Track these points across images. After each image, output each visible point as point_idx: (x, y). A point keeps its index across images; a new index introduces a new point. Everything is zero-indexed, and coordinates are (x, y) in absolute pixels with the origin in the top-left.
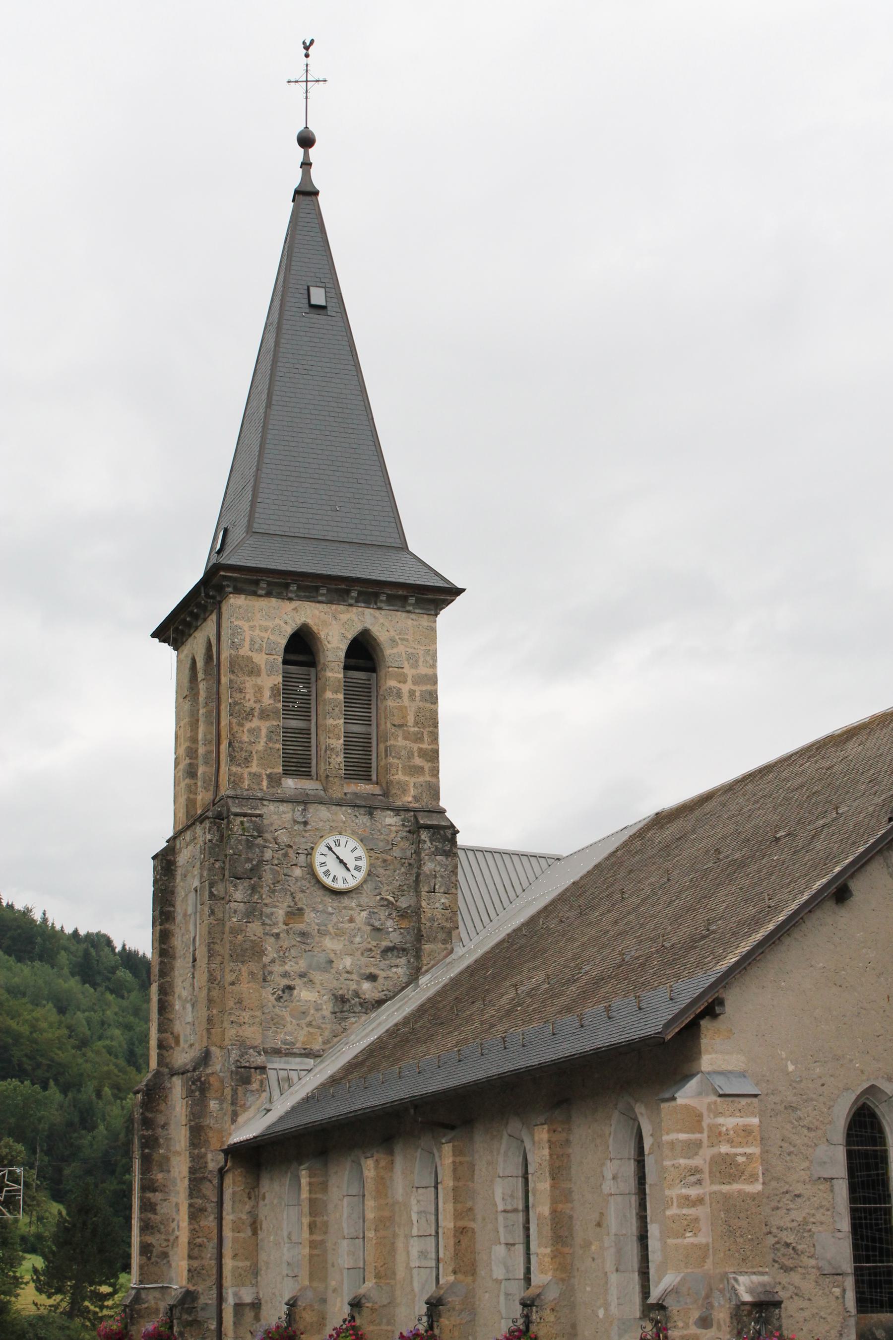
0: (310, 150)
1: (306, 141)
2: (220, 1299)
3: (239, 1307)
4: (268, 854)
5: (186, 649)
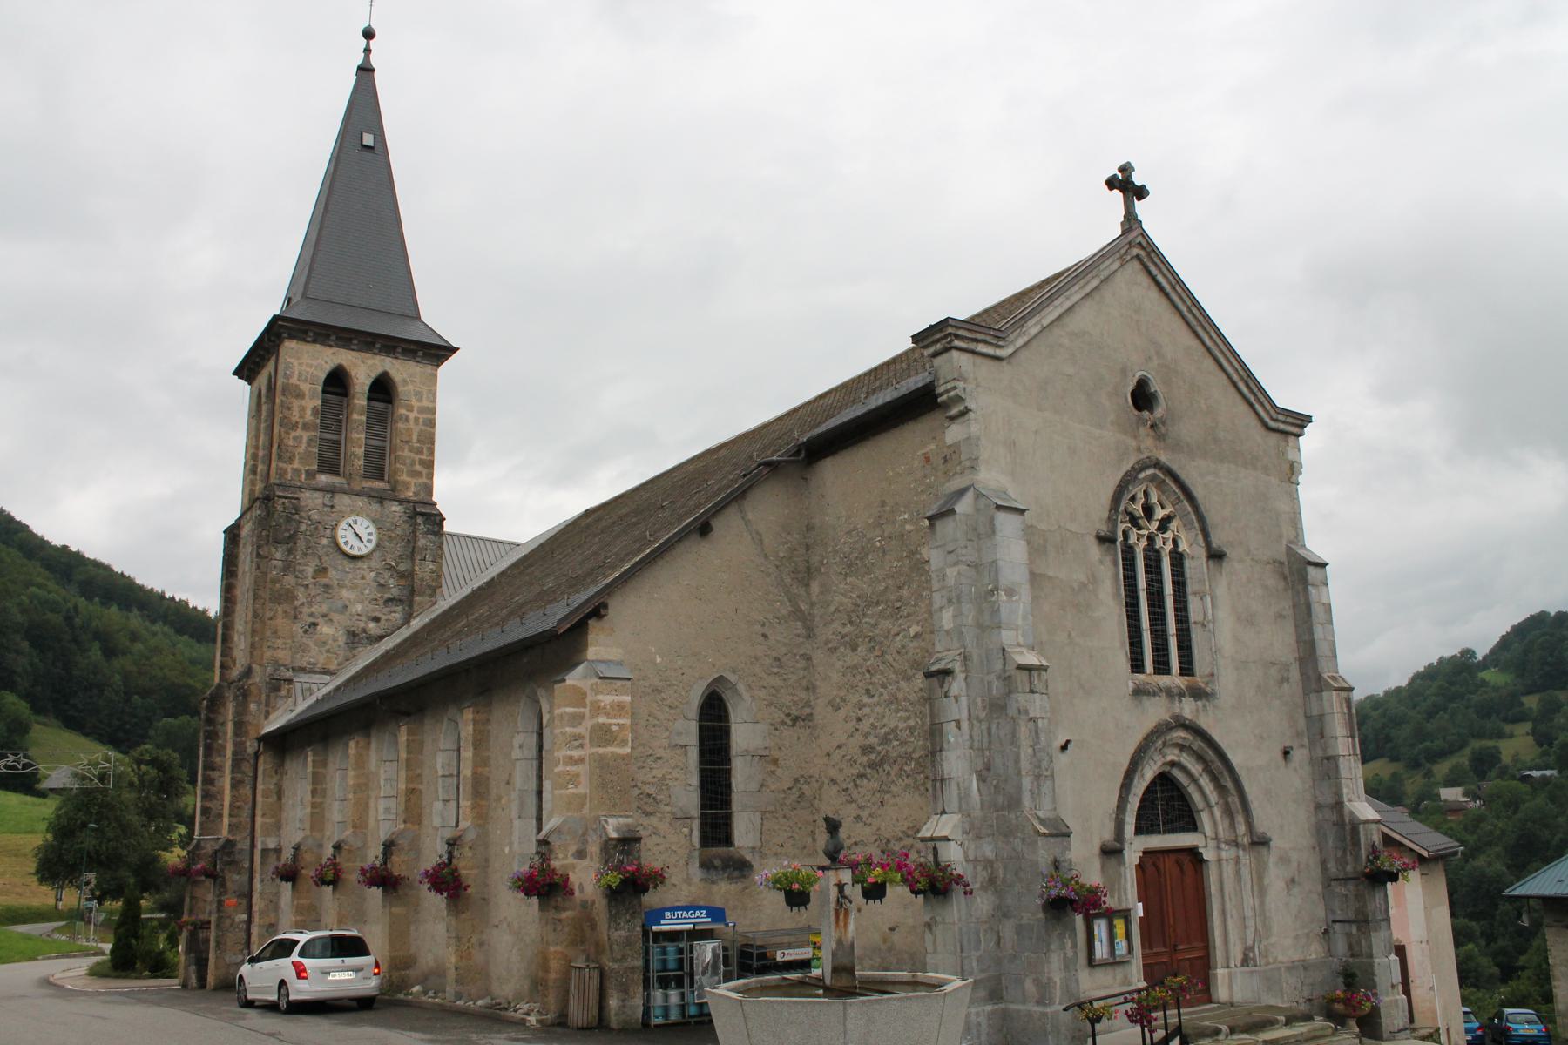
1: (369, 34)
2: (253, 845)
3: (265, 851)
4: (303, 527)
5: (256, 384)
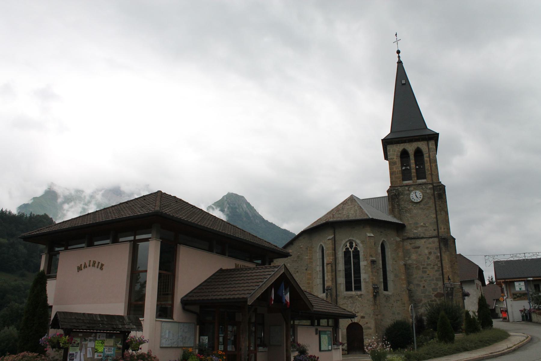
1: (398, 52)
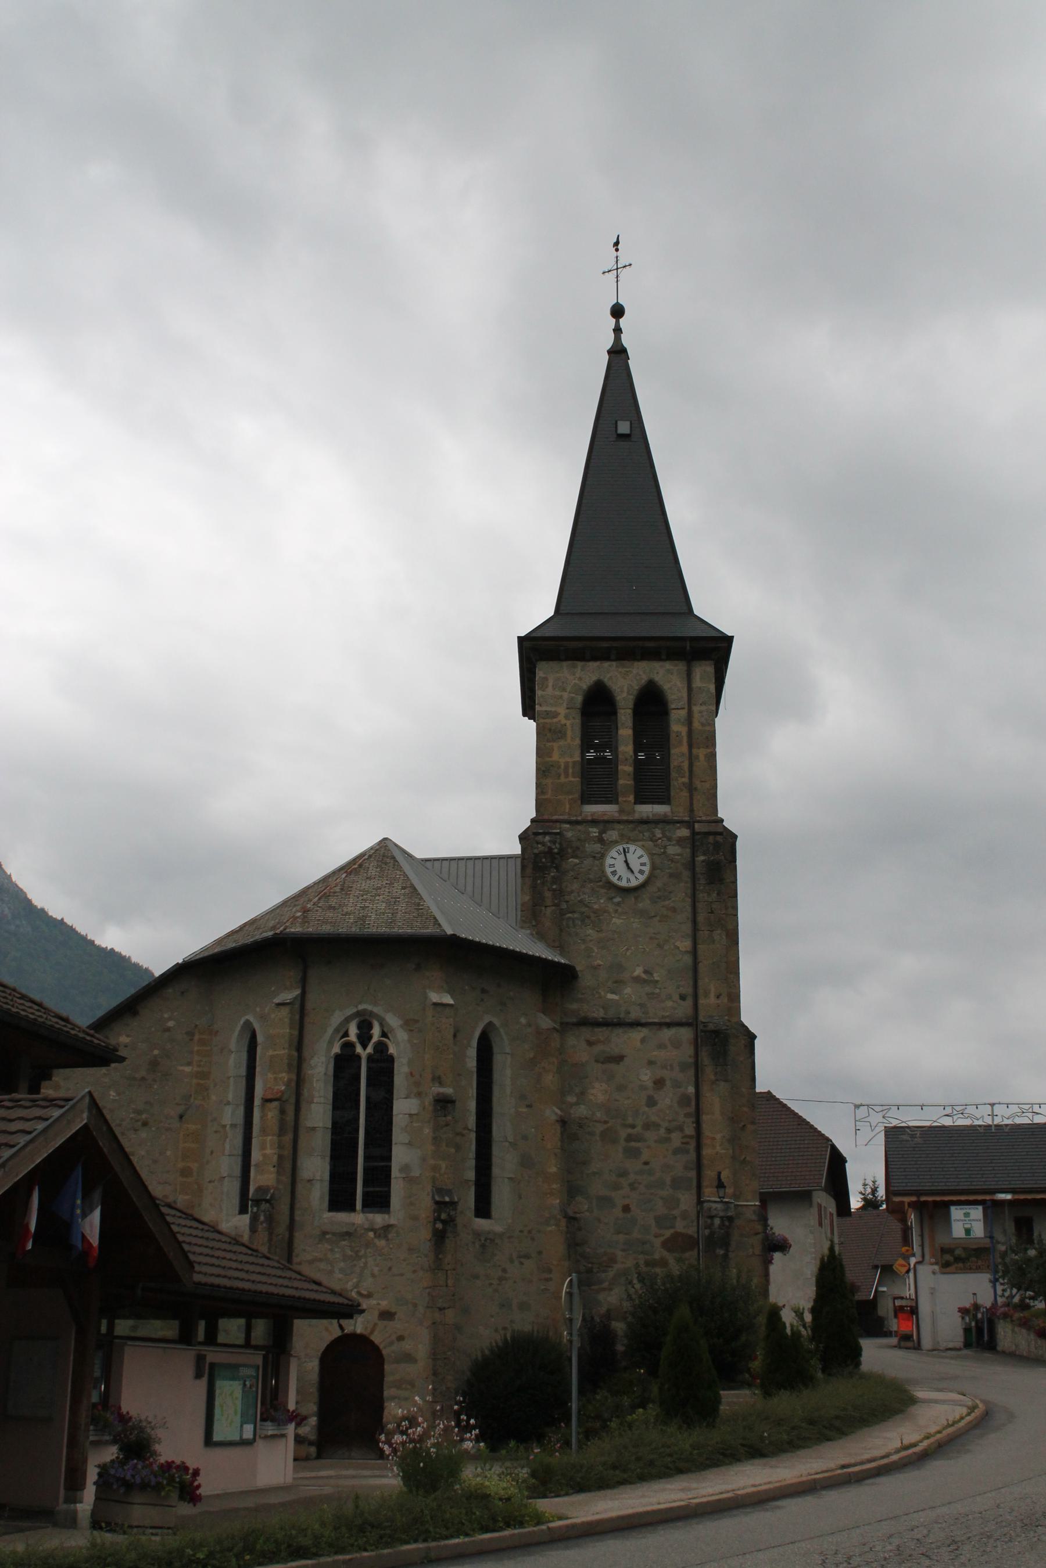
0: (621, 320)
1: (618, 312)
